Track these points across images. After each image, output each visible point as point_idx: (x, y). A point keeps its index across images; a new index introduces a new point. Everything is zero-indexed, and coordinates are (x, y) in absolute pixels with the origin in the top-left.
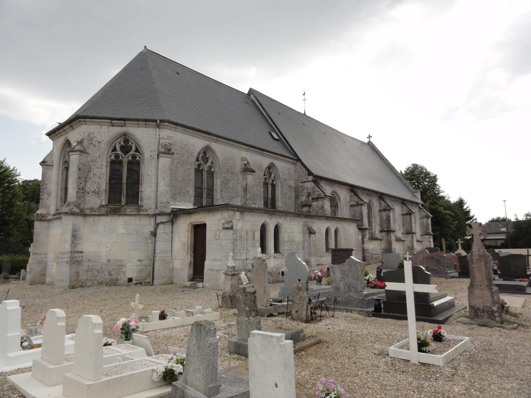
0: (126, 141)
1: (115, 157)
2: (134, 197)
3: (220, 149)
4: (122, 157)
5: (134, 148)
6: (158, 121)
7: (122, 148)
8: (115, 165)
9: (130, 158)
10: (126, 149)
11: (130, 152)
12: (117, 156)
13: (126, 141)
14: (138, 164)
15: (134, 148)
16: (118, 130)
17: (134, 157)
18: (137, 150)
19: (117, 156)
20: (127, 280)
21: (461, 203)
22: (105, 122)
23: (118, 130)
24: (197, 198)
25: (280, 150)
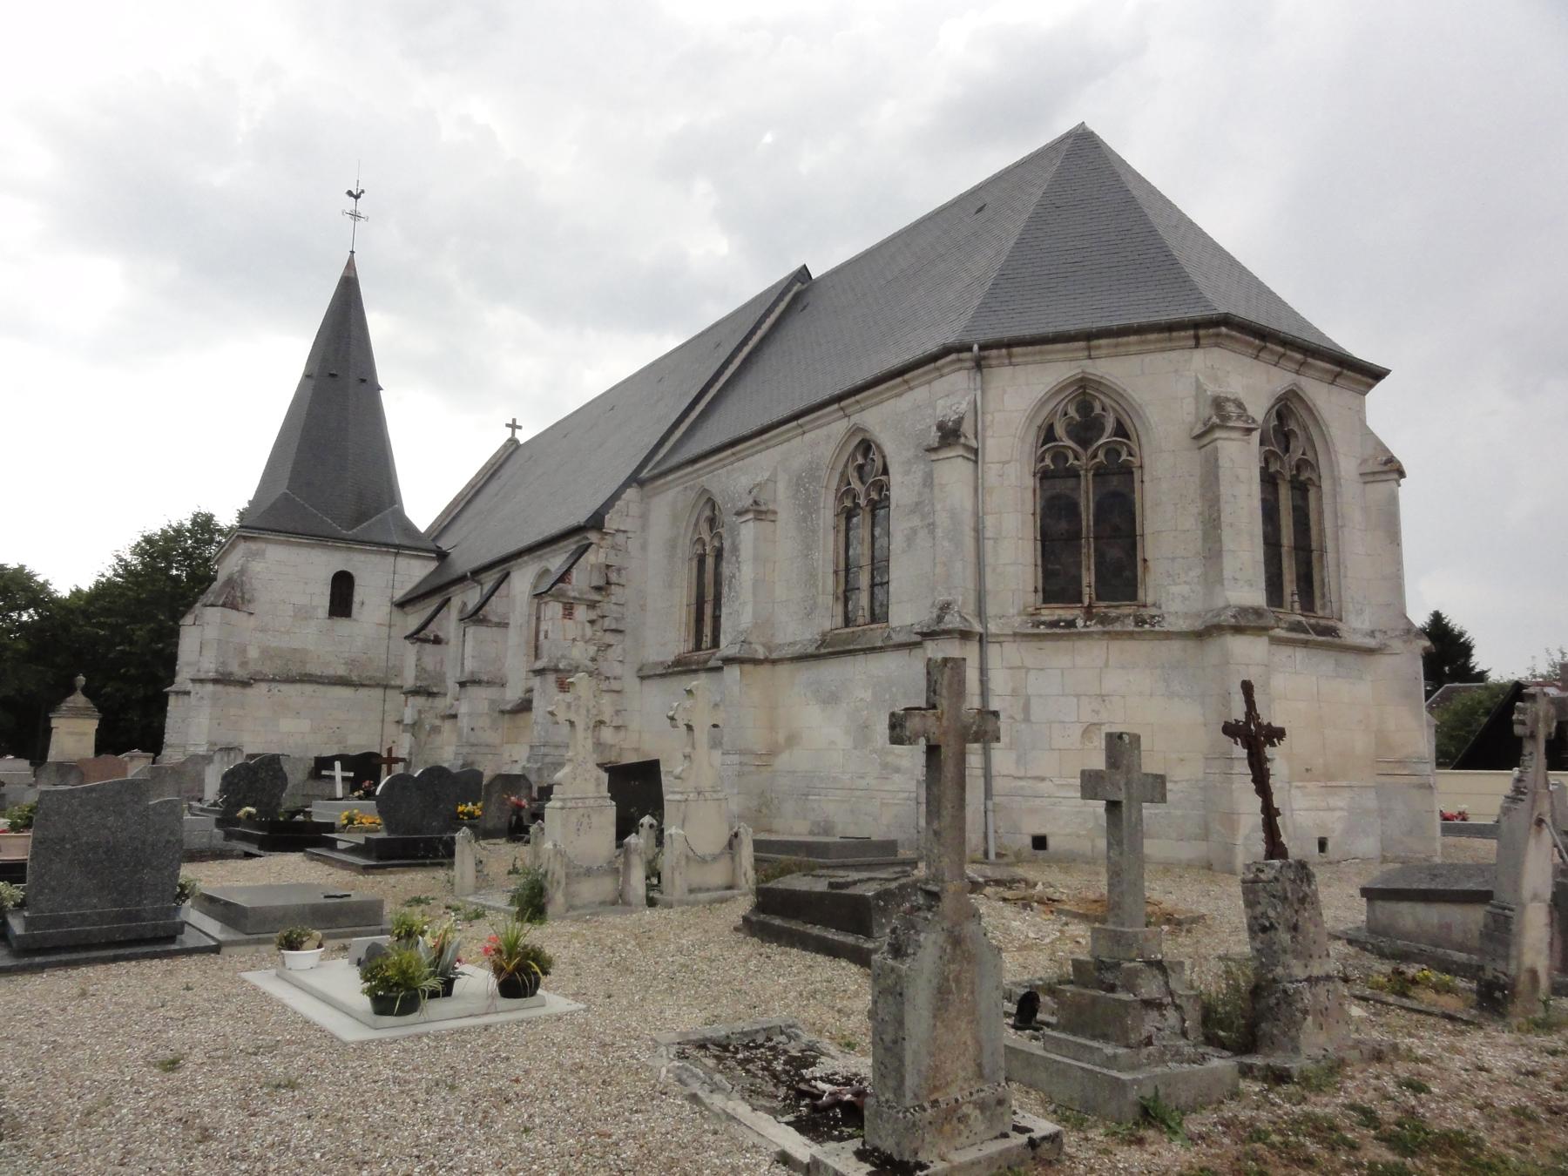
0: (1085, 407)
1: (1054, 460)
2: (1121, 577)
3: (1120, 371)
4: (1077, 458)
5: (1110, 425)
6: (976, 347)
7: (1073, 432)
8: (1053, 477)
9: (1101, 456)
10: (1086, 429)
11: (1100, 436)
12: (1059, 456)
13: (1085, 407)
14: (1127, 471)
15: (1110, 425)
16: (839, 428)
17: (1112, 452)
18: (1121, 430)
19: (1059, 456)
20: (1028, 841)
21: (22, 567)
22: (788, 431)
23: (839, 428)
24: (162, 673)
25: (489, 579)
